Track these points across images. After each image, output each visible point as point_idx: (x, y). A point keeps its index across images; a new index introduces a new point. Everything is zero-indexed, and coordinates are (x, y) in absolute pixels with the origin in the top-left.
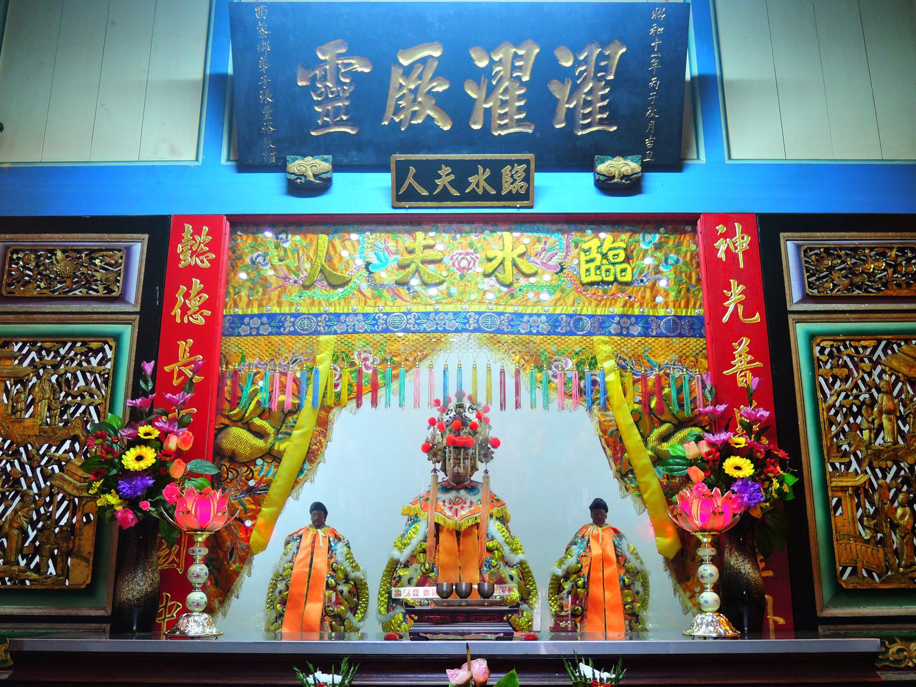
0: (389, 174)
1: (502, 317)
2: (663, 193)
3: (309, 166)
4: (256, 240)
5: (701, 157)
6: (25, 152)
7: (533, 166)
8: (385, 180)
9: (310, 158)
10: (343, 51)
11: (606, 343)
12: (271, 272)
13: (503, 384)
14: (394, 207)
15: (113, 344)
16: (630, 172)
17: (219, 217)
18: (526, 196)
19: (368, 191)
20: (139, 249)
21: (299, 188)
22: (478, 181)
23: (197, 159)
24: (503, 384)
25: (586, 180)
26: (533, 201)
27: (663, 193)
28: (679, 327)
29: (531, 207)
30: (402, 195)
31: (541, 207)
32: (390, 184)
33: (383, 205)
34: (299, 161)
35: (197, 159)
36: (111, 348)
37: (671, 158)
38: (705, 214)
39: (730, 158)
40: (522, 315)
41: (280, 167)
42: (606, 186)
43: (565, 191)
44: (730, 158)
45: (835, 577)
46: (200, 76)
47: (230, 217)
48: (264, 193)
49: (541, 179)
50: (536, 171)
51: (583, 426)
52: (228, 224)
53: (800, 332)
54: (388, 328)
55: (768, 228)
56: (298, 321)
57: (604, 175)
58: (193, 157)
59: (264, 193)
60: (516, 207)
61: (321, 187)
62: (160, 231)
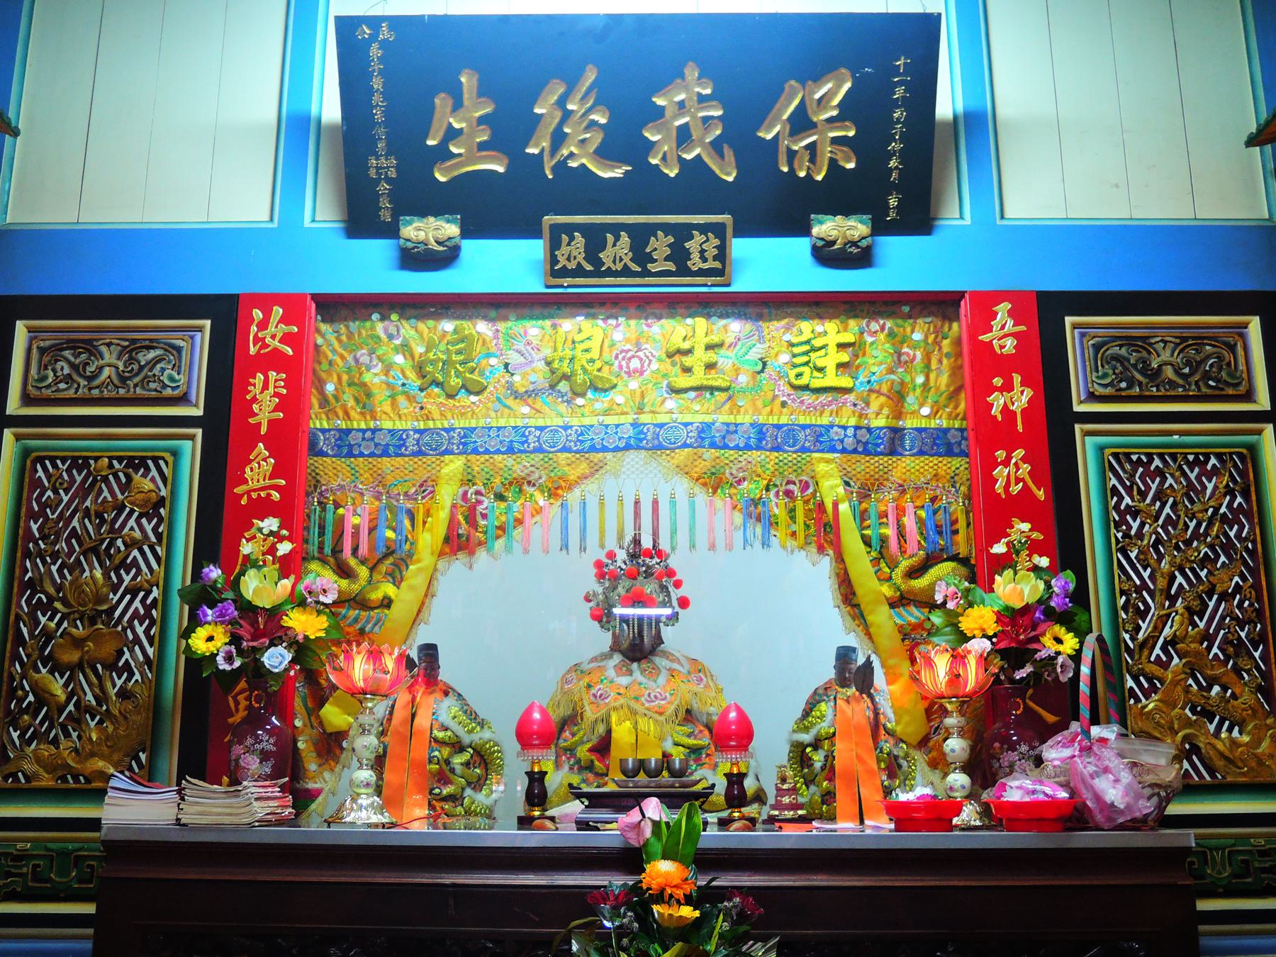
0: (541, 242)
1: (808, 431)
2: (903, 263)
3: (427, 230)
4: (759, 329)
5: (959, 212)
6: (15, 216)
7: (729, 231)
8: (535, 249)
9: (431, 219)
10: (708, 91)
11: (828, 461)
12: (379, 371)
13: (637, 515)
14: (548, 287)
15: (170, 459)
16: (856, 238)
17: (302, 297)
18: (721, 267)
19: (507, 263)
20: (199, 339)
21: (414, 259)
22: (618, 251)
23: (272, 219)
24: (637, 515)
25: (799, 247)
26: (730, 276)
27: (903, 263)
28: (937, 443)
29: (728, 285)
30: (555, 271)
31: (742, 283)
32: (542, 256)
33: (534, 284)
34: (418, 223)
35: (272, 219)
36: (166, 463)
37: (918, 217)
38: (974, 294)
39: (1002, 217)
40: (473, 430)
41: (391, 231)
42: (826, 255)
43: (771, 262)
44: (1002, 217)
45: (280, 822)
46: (269, 114)
47: (315, 297)
48: (370, 266)
49: (741, 247)
50: (735, 236)
51: (816, 573)
52: (314, 305)
53: (1088, 449)
54: (660, 443)
55: (1046, 310)
56: (546, 436)
57: (822, 239)
58: (267, 218)
59: (370, 266)
60: (705, 285)
61: (445, 258)
62: (226, 313)
